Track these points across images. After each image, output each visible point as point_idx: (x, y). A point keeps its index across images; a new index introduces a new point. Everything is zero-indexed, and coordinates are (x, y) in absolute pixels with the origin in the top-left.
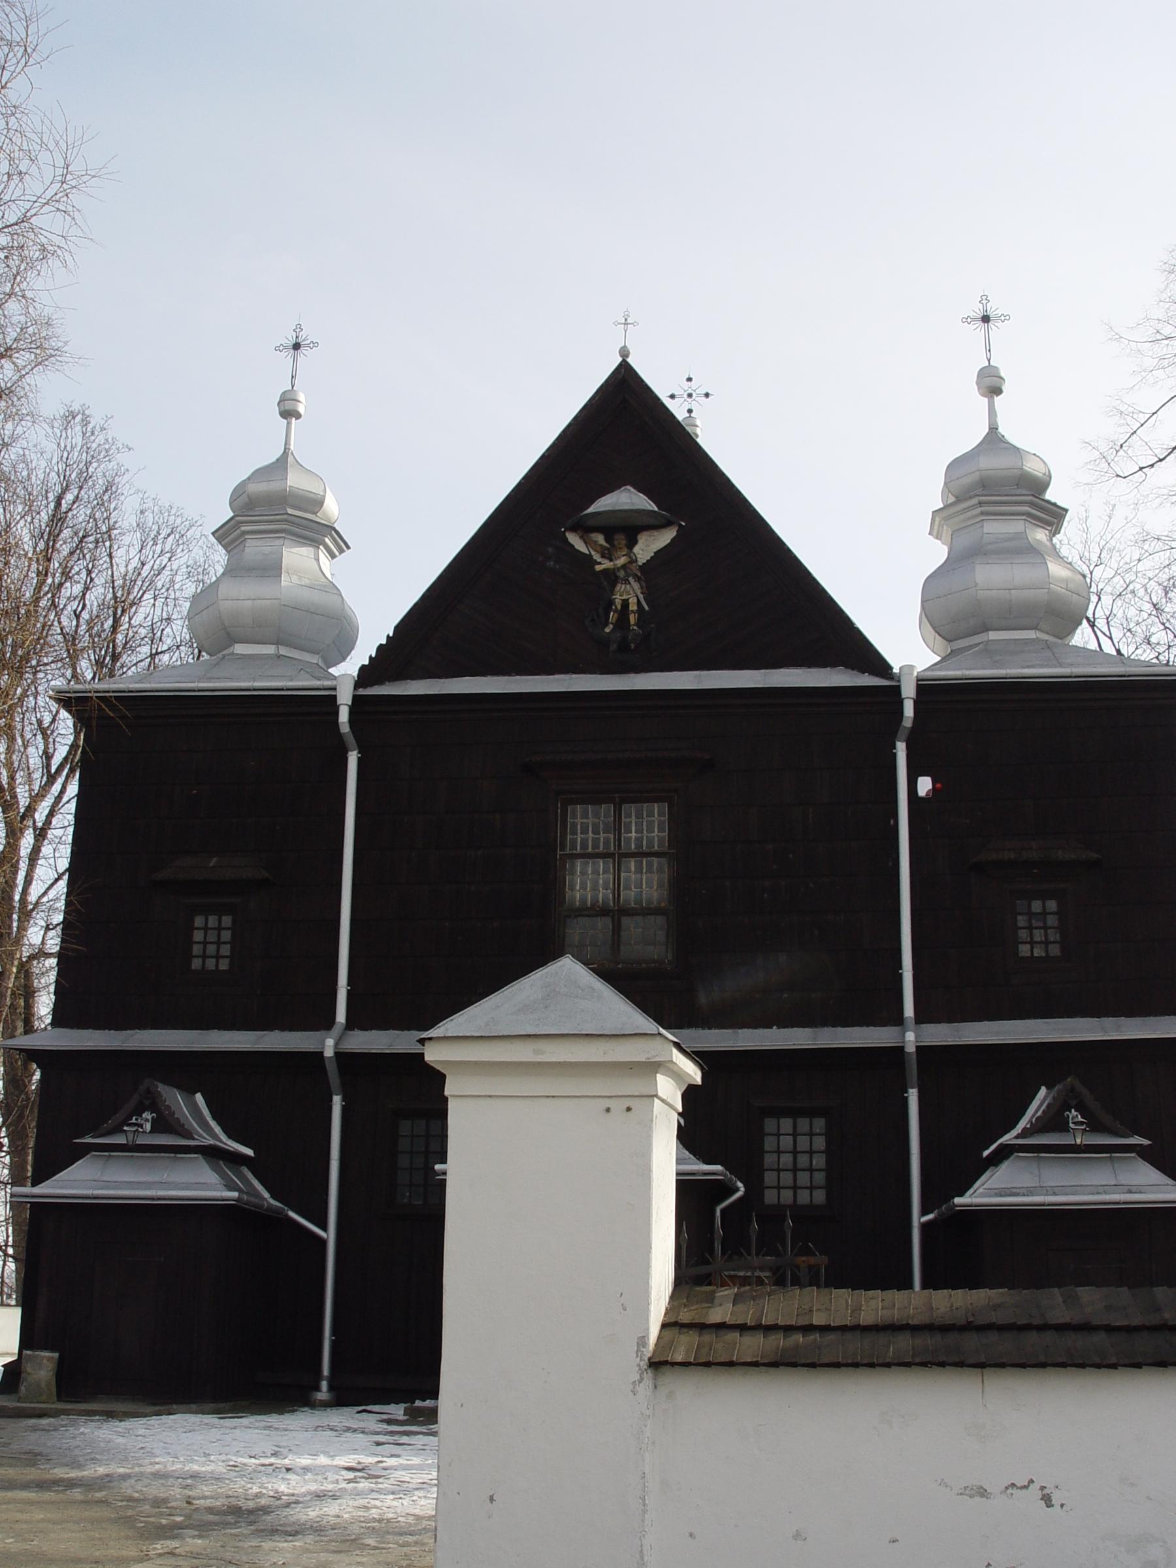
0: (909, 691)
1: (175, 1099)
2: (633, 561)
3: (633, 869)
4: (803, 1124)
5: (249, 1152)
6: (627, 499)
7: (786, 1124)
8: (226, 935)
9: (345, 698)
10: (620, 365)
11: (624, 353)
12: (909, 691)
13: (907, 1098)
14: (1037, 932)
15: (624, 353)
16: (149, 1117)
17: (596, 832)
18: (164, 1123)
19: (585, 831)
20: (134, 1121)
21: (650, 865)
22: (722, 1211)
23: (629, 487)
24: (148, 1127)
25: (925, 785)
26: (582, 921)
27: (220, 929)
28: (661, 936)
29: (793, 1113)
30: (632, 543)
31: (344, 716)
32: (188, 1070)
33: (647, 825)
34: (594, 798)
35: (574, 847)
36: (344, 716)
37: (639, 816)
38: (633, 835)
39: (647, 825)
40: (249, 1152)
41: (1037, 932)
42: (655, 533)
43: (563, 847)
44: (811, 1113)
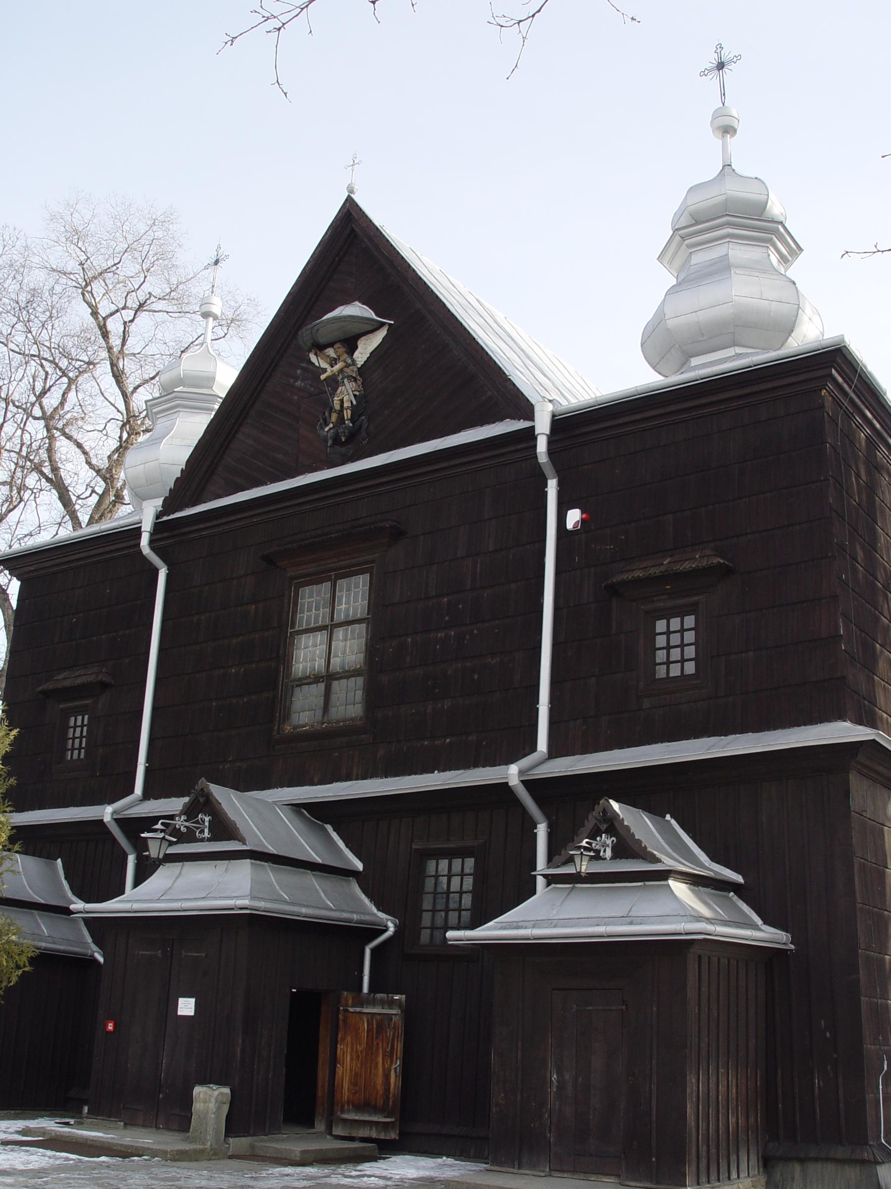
0: (542, 425)
1: (640, 823)
2: (354, 363)
3: (341, 638)
4: (457, 864)
5: (739, 879)
6: (357, 310)
7: (444, 864)
8: (690, 637)
9: (147, 526)
10: (346, 200)
11: (351, 190)
12: (542, 425)
13: (536, 834)
14: (676, 646)
15: (351, 190)
16: (609, 842)
17: (317, 609)
18: (627, 848)
19: (309, 610)
20: (584, 843)
21: (353, 632)
22: (373, 951)
23: (357, 303)
24: (609, 853)
25: (574, 517)
26: (305, 688)
27: (682, 631)
28: (359, 694)
29: (450, 854)
30: (128, 433)
31: (542, 446)
32: (639, 787)
33: (354, 596)
34: (316, 579)
35: (301, 624)
36: (542, 446)
37: (349, 590)
38: (343, 606)
39: (354, 596)
40: (739, 879)
41: (676, 646)
42: (370, 336)
43: (293, 626)
44: (463, 853)
